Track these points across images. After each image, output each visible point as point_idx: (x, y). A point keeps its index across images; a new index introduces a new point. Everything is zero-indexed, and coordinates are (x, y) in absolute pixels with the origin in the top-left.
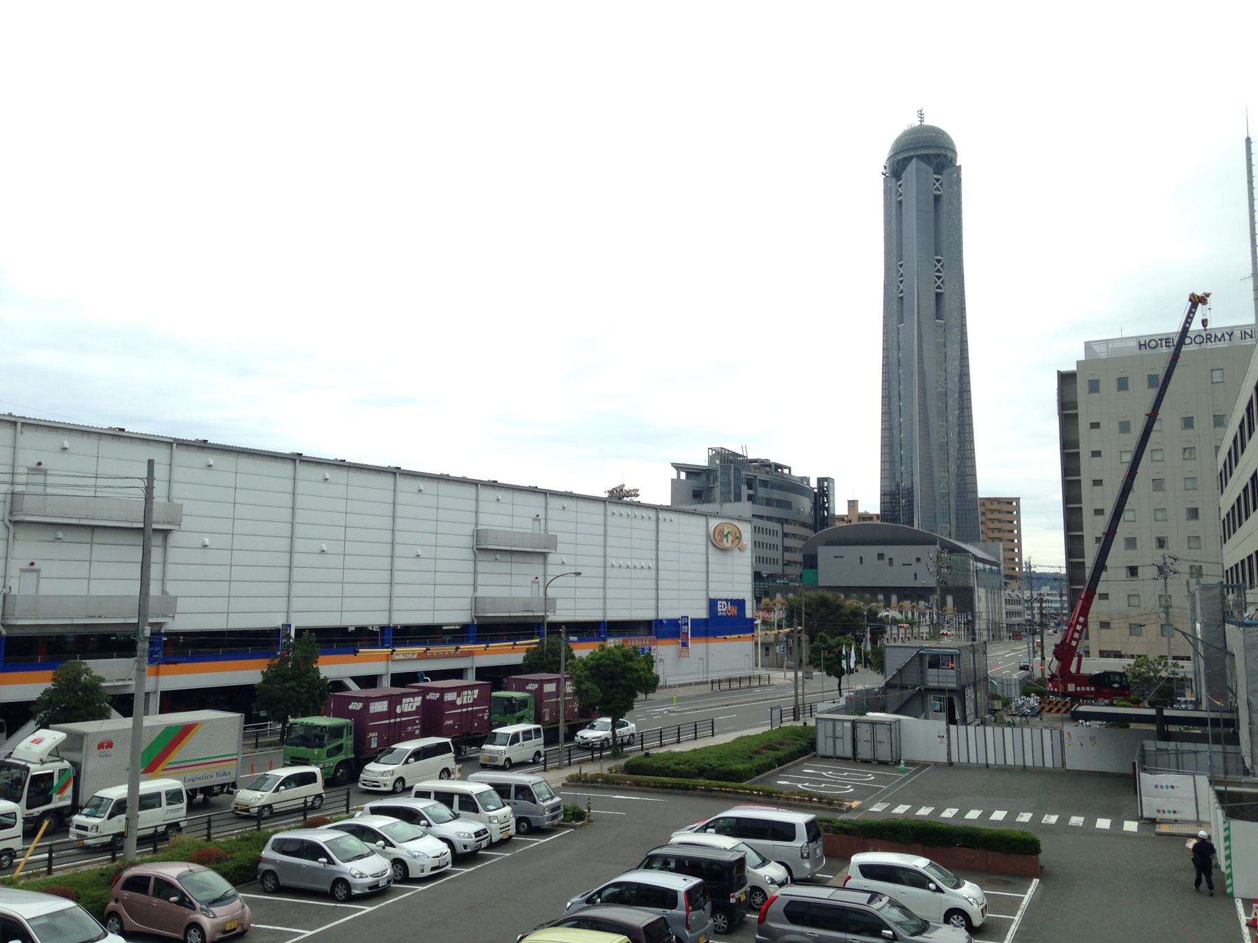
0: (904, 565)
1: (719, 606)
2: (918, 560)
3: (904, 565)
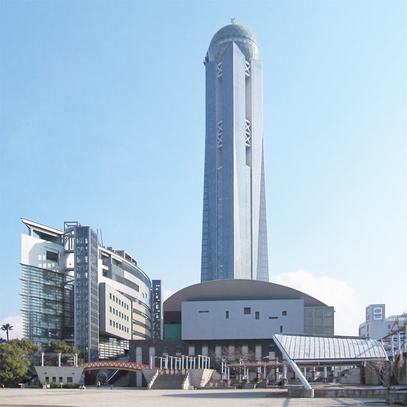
0: (270, 318)
1: (128, 346)
2: (284, 313)
3: (270, 318)
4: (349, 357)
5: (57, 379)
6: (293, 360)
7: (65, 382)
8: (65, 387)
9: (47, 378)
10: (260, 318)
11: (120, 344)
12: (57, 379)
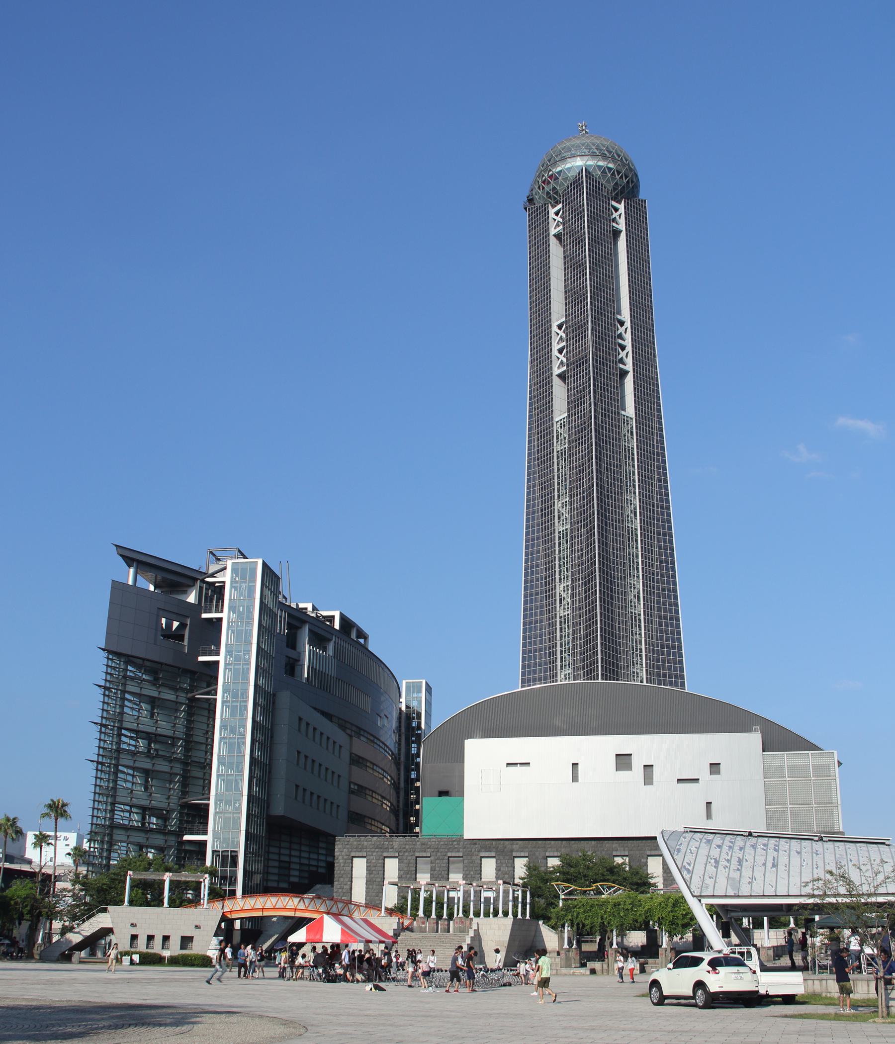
5: (158, 941)
6: (699, 898)
7: (174, 950)
8: (175, 961)
9: (134, 937)
10: (654, 782)
11: (280, 867)
12: (158, 941)
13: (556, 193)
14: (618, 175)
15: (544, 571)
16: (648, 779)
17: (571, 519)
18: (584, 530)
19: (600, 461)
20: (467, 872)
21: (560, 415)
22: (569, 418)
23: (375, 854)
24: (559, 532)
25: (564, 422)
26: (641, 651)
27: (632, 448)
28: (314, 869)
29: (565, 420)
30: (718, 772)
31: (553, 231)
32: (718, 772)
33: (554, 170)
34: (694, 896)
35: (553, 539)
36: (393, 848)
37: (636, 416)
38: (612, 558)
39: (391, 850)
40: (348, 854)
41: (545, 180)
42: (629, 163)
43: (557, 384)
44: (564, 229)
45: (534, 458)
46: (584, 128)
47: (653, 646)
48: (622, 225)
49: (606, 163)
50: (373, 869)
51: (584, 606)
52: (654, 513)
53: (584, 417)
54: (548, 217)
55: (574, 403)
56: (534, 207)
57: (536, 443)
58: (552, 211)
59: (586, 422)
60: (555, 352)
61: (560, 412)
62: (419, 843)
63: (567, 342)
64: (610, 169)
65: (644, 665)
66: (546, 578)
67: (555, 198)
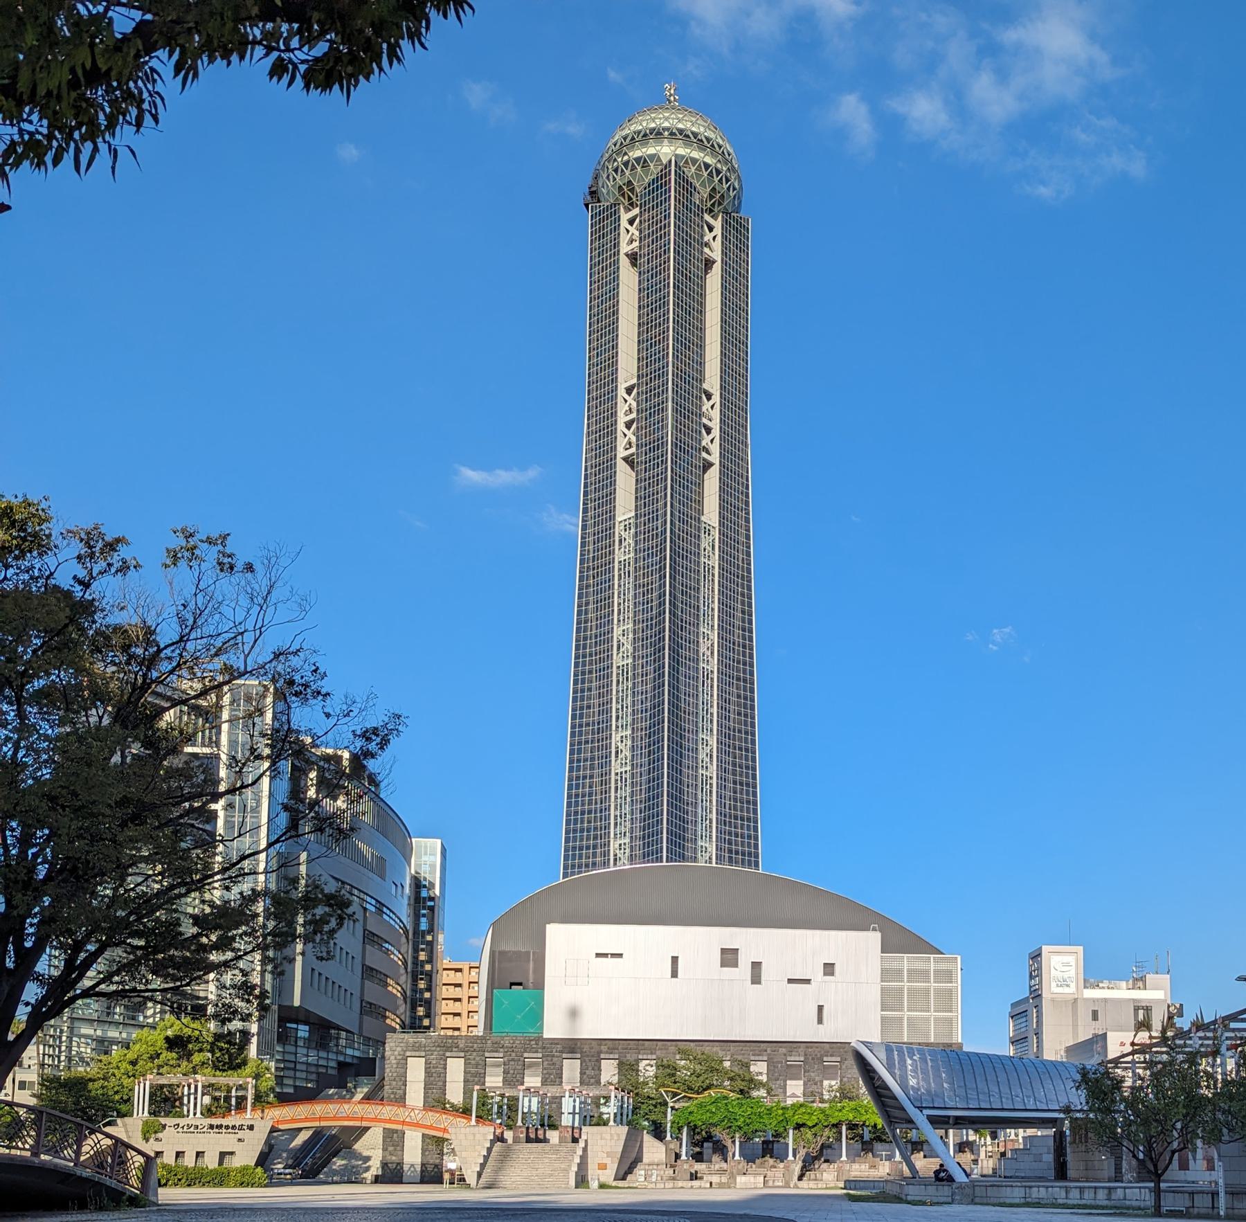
2: (829, 969)
3: (790, 981)
4: (1012, 1107)
10: (763, 982)
13: (632, 190)
14: (706, 171)
15: (596, 714)
16: (756, 979)
17: (634, 652)
18: (650, 668)
19: (675, 580)
20: (547, 1076)
21: (624, 514)
22: (636, 519)
23: (436, 1053)
24: (618, 667)
25: (630, 524)
26: (711, 822)
27: (713, 567)
28: (322, 1070)
29: (631, 521)
30: (832, 974)
31: (625, 248)
32: (832, 974)
33: (631, 154)
34: (916, 1107)
35: (609, 676)
36: (457, 1047)
37: (720, 525)
38: (683, 706)
39: (456, 1049)
40: (402, 1053)
41: (617, 168)
42: (723, 152)
43: (622, 469)
44: (640, 247)
45: (588, 567)
46: (672, 92)
47: (725, 816)
48: (716, 253)
49: (702, 155)
50: (433, 1070)
51: (647, 763)
52: (734, 653)
53: (657, 520)
54: (619, 225)
55: (644, 498)
56: (600, 206)
57: (591, 547)
58: (625, 217)
59: (659, 527)
60: (621, 426)
61: (625, 507)
62: (489, 1042)
63: (638, 414)
64: (707, 166)
65: (714, 839)
66: (599, 724)
67: (630, 199)
